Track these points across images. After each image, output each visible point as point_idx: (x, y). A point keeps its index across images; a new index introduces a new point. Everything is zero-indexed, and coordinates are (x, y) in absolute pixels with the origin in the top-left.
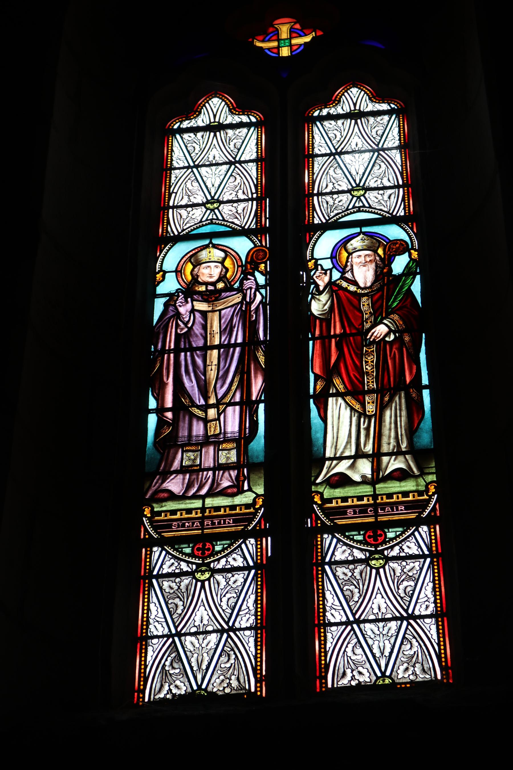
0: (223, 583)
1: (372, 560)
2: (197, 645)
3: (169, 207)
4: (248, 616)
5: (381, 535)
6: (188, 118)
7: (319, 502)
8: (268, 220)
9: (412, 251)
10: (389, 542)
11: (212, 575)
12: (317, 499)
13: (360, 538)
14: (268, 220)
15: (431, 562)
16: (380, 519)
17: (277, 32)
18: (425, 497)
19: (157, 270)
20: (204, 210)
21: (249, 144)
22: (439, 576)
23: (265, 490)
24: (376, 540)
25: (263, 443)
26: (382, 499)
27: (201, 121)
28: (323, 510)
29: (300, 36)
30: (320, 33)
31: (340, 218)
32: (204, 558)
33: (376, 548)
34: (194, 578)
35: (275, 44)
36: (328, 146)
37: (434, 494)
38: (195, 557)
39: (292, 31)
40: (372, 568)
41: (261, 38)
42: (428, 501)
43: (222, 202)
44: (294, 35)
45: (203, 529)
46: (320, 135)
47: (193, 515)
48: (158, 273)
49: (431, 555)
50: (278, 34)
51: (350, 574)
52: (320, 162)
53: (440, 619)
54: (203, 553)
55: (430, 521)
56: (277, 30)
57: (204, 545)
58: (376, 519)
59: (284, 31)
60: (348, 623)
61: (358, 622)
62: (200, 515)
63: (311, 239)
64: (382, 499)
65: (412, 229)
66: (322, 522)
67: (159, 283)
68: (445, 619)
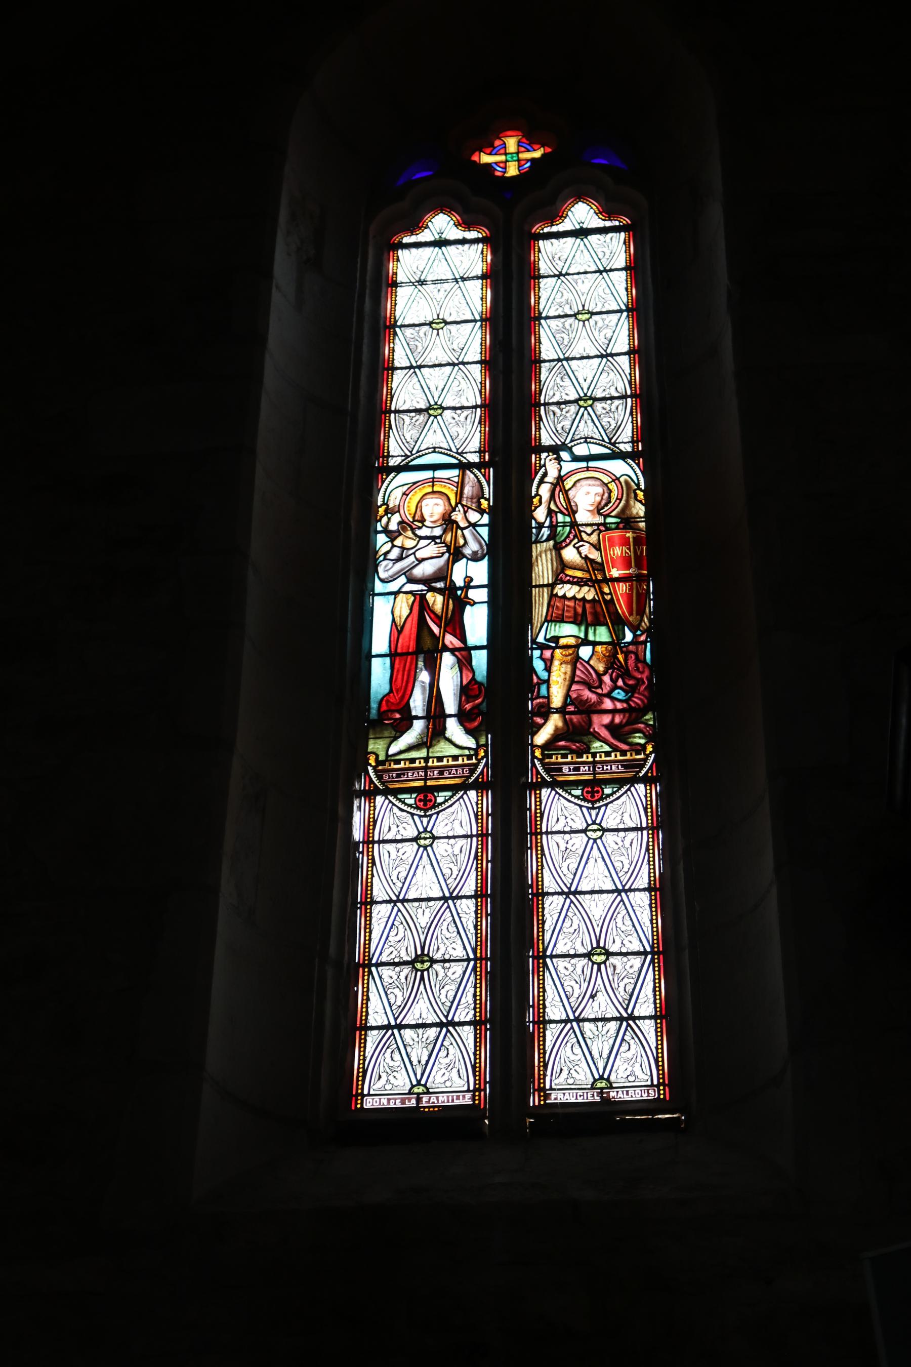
0: (441, 974)
1: (593, 955)
2: (417, 1039)
3: (390, 412)
4: (467, 1010)
5: (431, 801)
6: (412, 233)
7: (540, 757)
8: (490, 864)
9: (638, 492)
10: (606, 798)
11: (431, 966)
12: (372, 761)
13: (411, 801)
14: (490, 864)
15: (652, 961)
16: (598, 777)
17: (504, 145)
18: (474, 761)
19: (379, 503)
20: (427, 416)
21: (473, 259)
22: (659, 975)
23: (489, 596)
24: (593, 796)
25: (485, 673)
26: (601, 757)
27: (425, 236)
28: (543, 765)
29: (528, 151)
30: (549, 150)
31: (412, 460)
32: (593, 803)
33: (593, 805)
34: (414, 967)
35: (503, 158)
36: (564, 1006)
37: (651, 753)
38: (417, 808)
39: (519, 144)
40: (593, 963)
41: (488, 151)
42: (645, 760)
43: (444, 409)
44: (523, 149)
45: (425, 780)
46: (554, 922)
47: (417, 764)
48: (535, 497)
49: (653, 953)
50: (505, 147)
51: (571, 969)
52: (554, 1031)
53: (662, 1097)
54: (425, 805)
55: (646, 780)
56: (504, 143)
57: (426, 797)
58: (425, 783)
59: (512, 143)
60: (567, 1021)
61: (578, 1020)
62: (423, 764)
63: (383, 482)
64: (601, 757)
65: (638, 465)
66: (542, 777)
67: (536, 508)
68: (664, 1021)
